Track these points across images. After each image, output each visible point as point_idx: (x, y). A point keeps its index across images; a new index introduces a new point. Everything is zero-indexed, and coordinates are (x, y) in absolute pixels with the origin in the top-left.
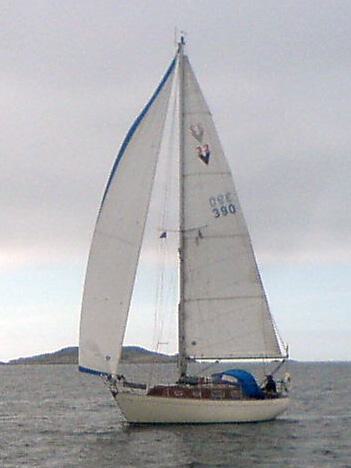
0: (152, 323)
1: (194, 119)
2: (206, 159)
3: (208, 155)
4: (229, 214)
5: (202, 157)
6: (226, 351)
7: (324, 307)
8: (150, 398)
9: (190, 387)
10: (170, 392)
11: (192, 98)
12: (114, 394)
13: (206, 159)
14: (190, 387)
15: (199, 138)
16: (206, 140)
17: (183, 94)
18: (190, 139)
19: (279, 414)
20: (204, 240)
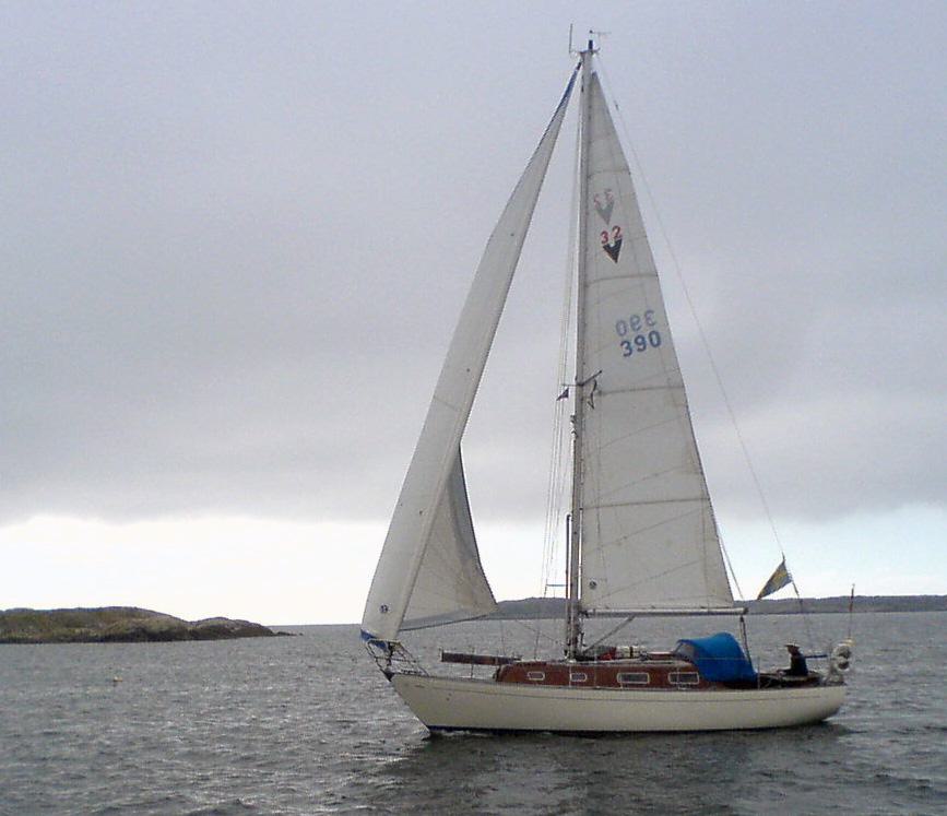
0: (523, 559)
1: (600, 182)
2: (614, 252)
3: (618, 243)
4: (635, 352)
5: (607, 248)
6: (650, 608)
7: (813, 539)
8: (499, 688)
9: (599, 669)
10: (555, 676)
11: (600, 146)
12: (389, 675)
13: (614, 252)
14: (599, 669)
15: (606, 215)
16: (615, 220)
17: (588, 142)
18: (595, 217)
19: (834, 712)
20: (606, 400)
